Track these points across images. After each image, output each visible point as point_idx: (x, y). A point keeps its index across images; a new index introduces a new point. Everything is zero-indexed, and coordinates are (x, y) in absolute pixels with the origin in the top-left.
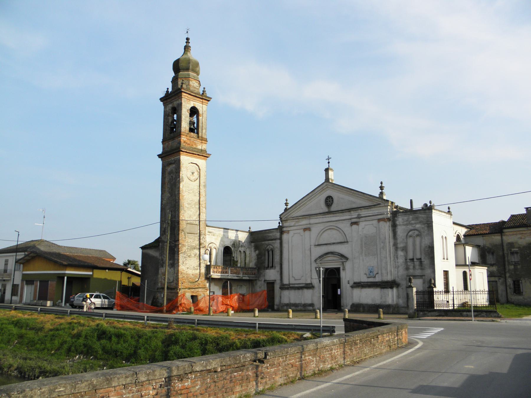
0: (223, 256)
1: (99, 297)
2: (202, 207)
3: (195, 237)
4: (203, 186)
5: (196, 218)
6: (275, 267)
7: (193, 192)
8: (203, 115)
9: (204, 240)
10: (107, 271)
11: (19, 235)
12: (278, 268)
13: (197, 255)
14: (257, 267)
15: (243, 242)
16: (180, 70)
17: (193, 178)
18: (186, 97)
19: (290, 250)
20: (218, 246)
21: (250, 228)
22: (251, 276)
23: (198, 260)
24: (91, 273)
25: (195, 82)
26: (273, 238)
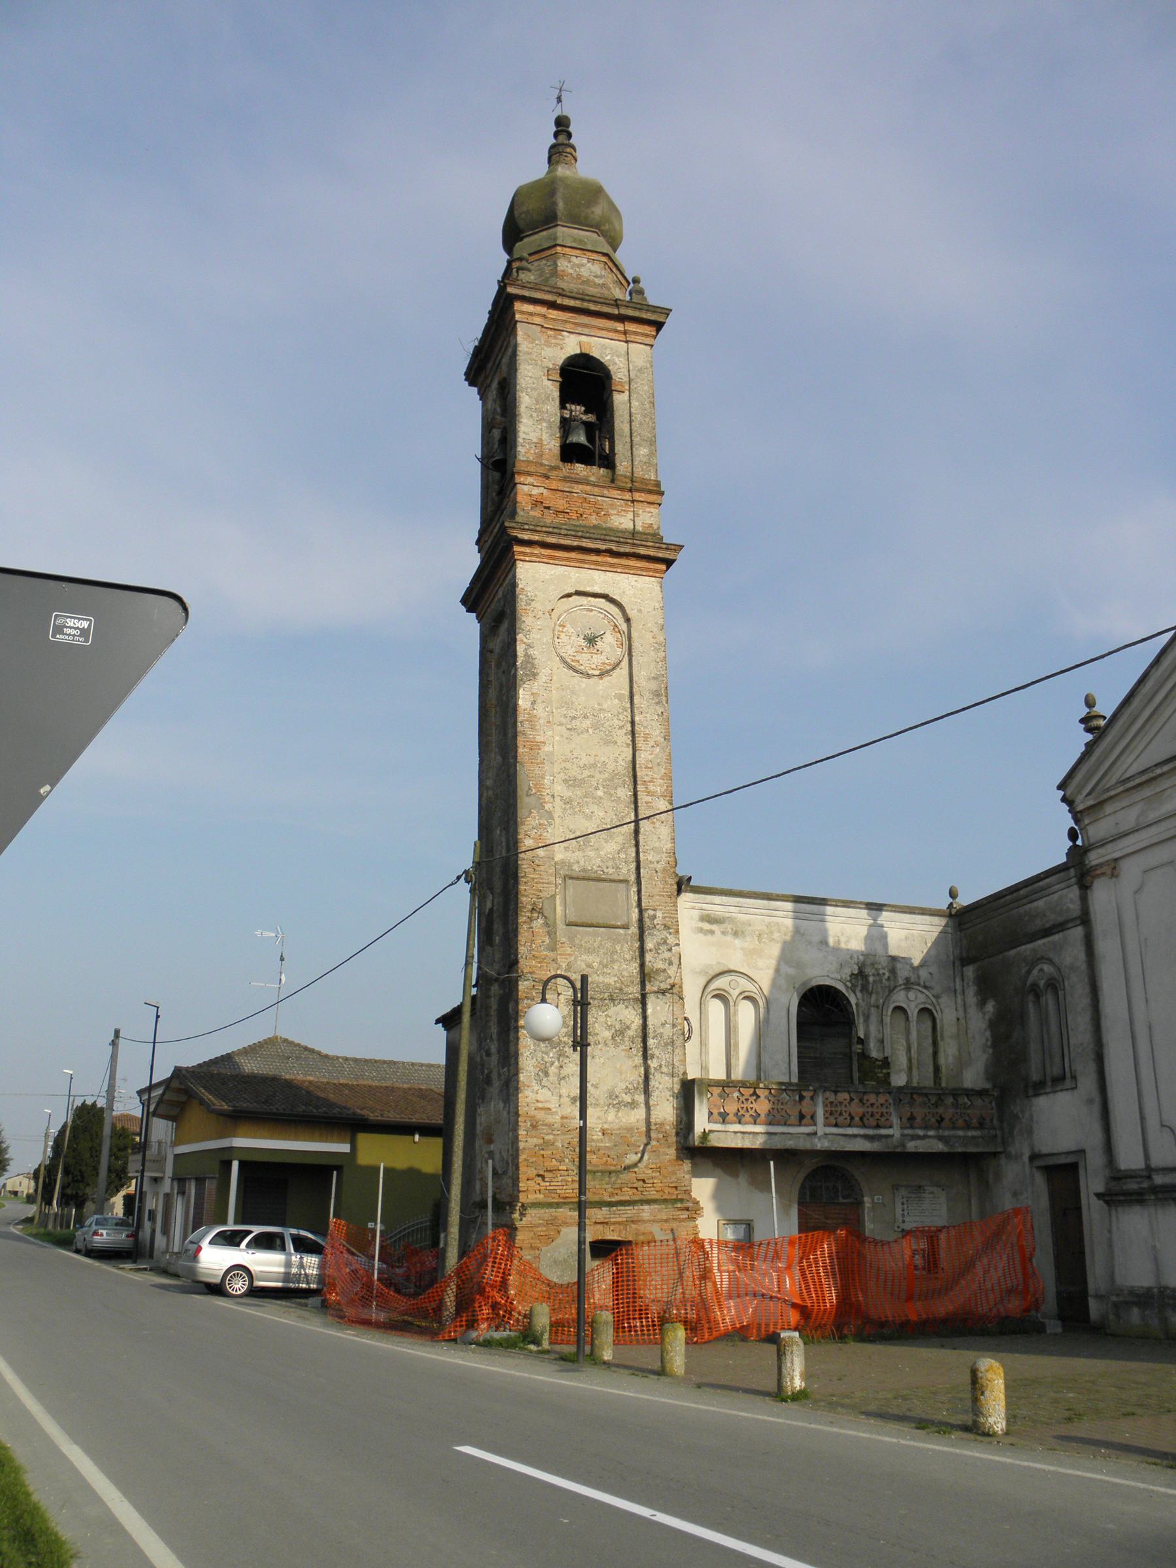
0: (800, 1038)
1: (278, 1242)
2: (649, 793)
3: (616, 941)
4: (647, 695)
5: (616, 847)
6: (1074, 1078)
7: (596, 726)
8: (633, 386)
9: (667, 955)
10: (417, 1137)
11: (158, 1017)
12: (1087, 1083)
13: (631, 1033)
14: (994, 1086)
15: (916, 962)
16: (521, 231)
17: (591, 661)
18: (537, 320)
19: (1135, 969)
20: (766, 986)
21: (953, 894)
22: (960, 1133)
23: (639, 1060)
24: (345, 1148)
25: (585, 261)
26: (1052, 919)
